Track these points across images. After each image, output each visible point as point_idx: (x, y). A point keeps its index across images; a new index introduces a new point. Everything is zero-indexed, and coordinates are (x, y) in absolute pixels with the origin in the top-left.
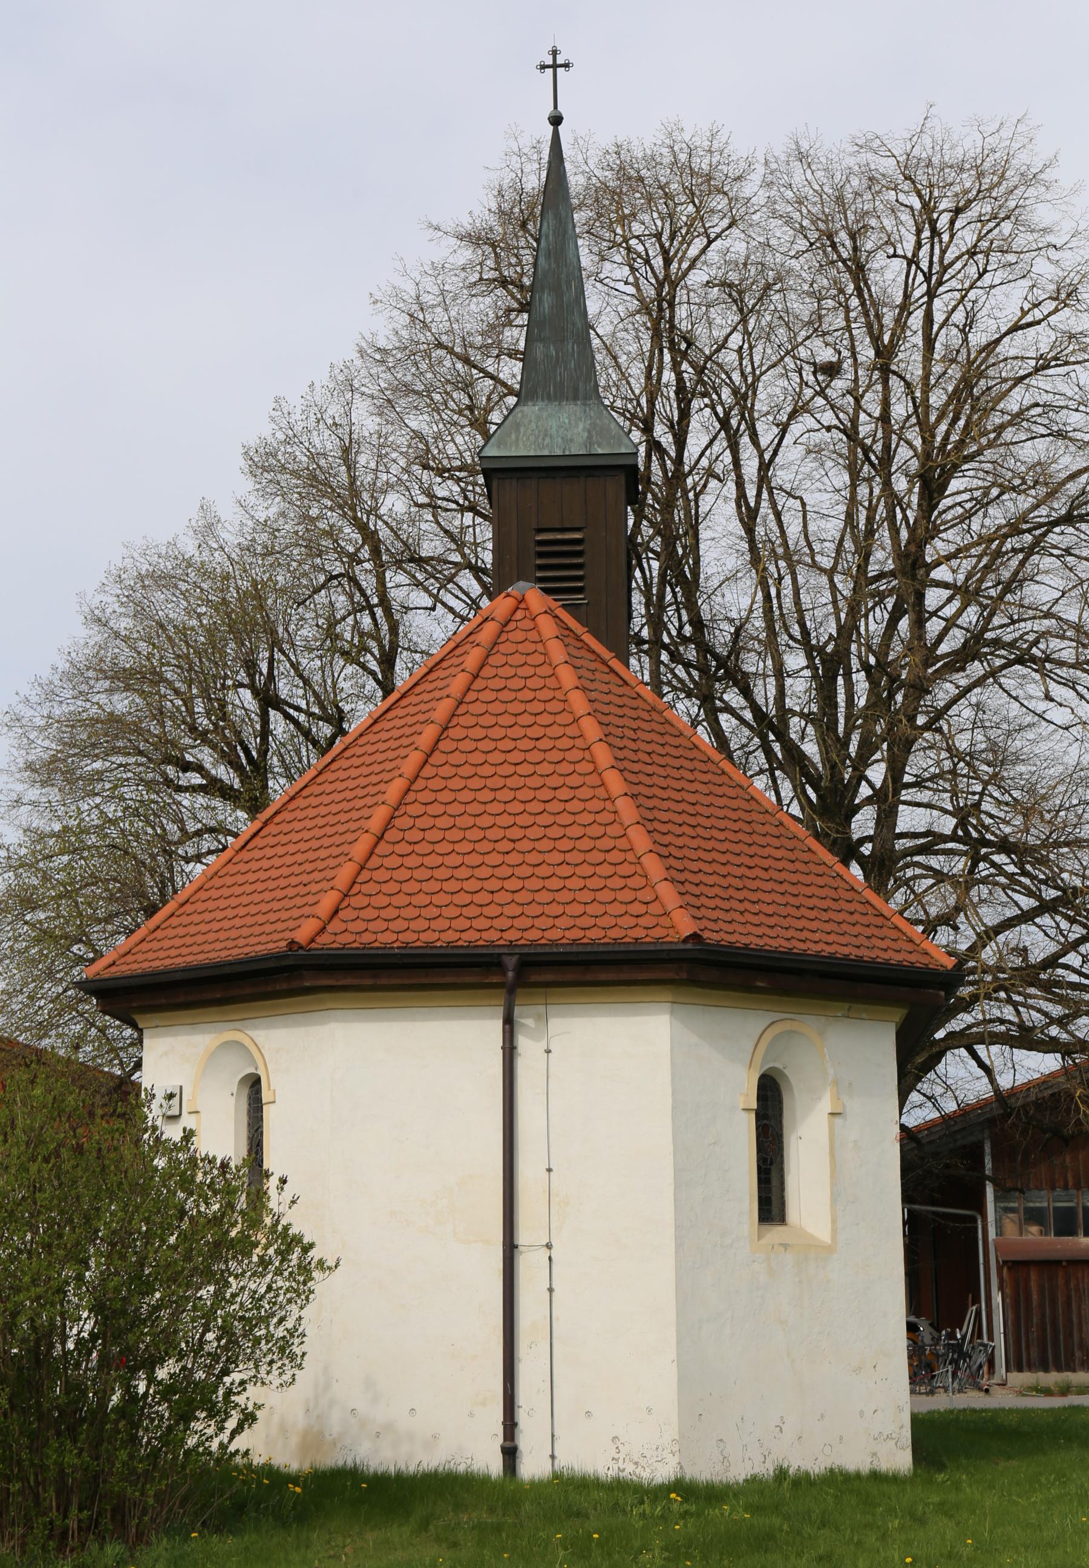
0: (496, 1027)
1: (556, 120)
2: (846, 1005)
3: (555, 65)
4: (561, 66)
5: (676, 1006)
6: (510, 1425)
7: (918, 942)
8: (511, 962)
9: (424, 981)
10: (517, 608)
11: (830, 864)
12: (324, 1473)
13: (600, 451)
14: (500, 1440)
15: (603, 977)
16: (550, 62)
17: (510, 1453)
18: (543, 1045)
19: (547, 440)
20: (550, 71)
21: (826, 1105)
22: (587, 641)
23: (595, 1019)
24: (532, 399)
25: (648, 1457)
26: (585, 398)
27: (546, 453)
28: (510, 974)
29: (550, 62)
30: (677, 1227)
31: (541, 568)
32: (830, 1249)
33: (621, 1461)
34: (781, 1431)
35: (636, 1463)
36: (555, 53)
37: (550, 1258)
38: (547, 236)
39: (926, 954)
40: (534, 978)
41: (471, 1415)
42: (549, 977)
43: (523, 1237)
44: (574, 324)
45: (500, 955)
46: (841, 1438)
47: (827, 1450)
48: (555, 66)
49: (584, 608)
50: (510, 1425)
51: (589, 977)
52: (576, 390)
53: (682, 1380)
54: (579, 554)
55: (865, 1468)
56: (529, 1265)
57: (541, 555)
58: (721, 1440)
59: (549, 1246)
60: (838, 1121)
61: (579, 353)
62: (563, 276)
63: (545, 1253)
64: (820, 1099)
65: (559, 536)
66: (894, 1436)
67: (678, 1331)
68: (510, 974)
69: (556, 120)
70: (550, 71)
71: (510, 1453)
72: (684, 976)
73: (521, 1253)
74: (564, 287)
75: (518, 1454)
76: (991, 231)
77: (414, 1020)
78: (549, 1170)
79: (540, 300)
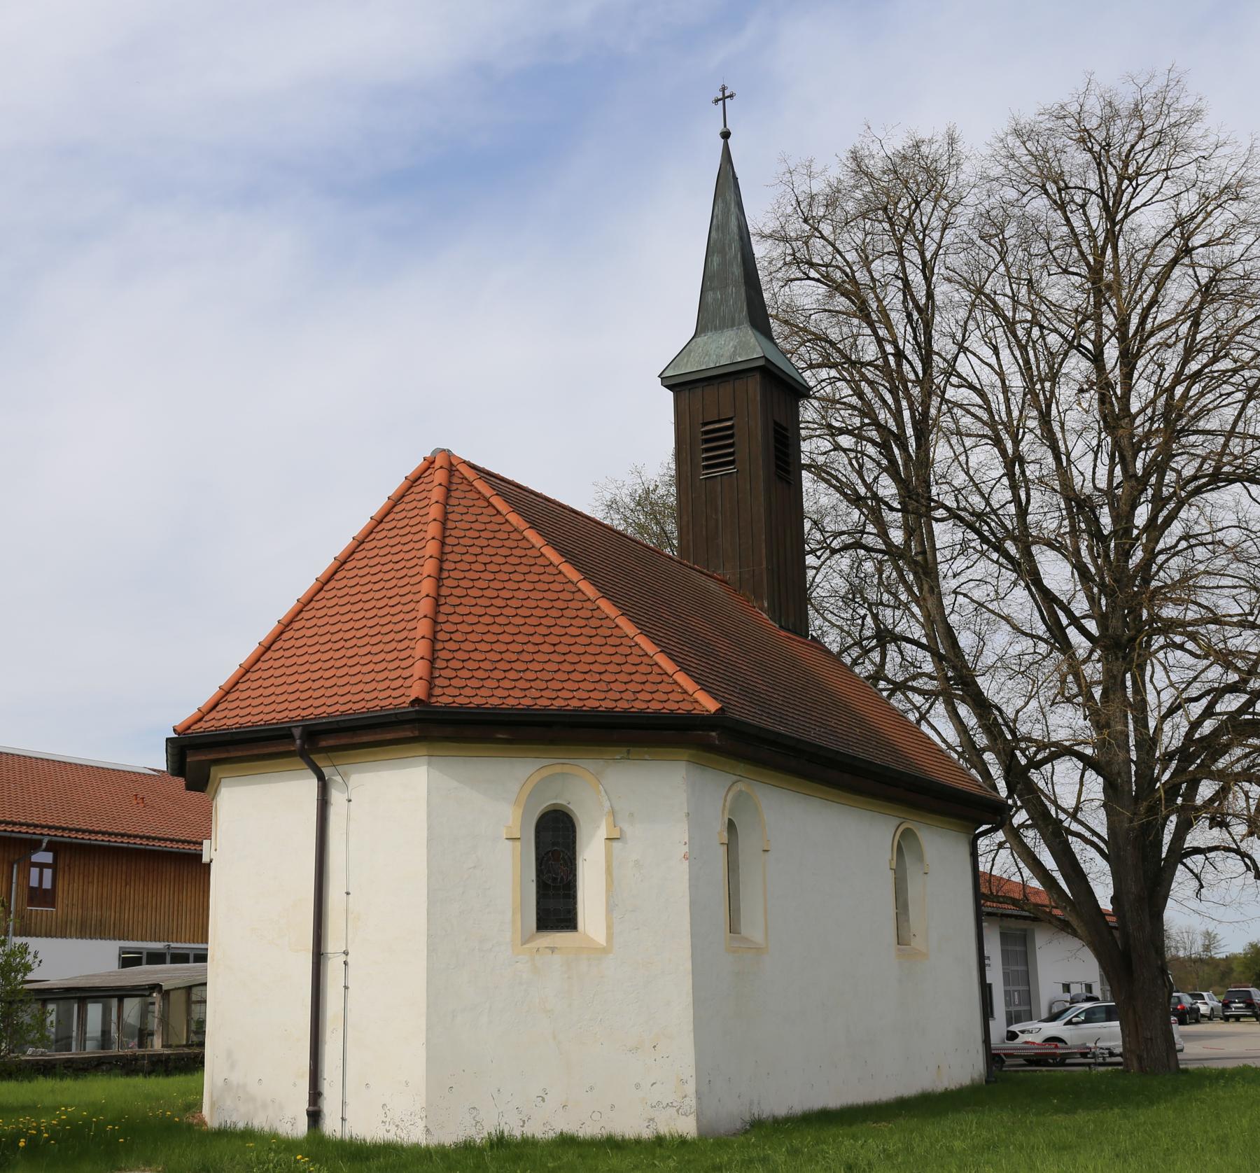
0: (312, 784)
1: (726, 135)
2: (625, 749)
3: (724, 97)
4: (728, 97)
5: (433, 758)
6: (315, 1094)
7: (691, 693)
8: (297, 732)
9: (256, 752)
10: (429, 468)
11: (631, 635)
12: (829, 1111)
13: (740, 360)
14: (306, 1106)
15: (365, 739)
16: (720, 96)
17: (315, 1116)
18: (346, 797)
19: (707, 358)
20: (721, 103)
21: (602, 833)
22: (480, 488)
23: (380, 773)
24: (704, 332)
25: (405, 1120)
26: (739, 325)
27: (704, 367)
28: (298, 742)
29: (721, 96)
30: (429, 936)
31: (707, 450)
32: (605, 951)
33: (387, 1123)
34: (543, 1100)
35: (397, 1126)
36: (723, 89)
37: (346, 963)
38: (717, 216)
39: (697, 702)
40: (323, 744)
41: (295, 1085)
42: (331, 742)
43: (333, 945)
44: (733, 273)
45: (290, 727)
46: (613, 1107)
47: (596, 1116)
48: (724, 99)
49: (735, 475)
50: (315, 1094)
51: (356, 740)
52: (733, 320)
53: (429, 1060)
54: (731, 436)
55: (647, 1134)
56: (333, 968)
57: (706, 441)
58: (474, 1108)
59: (346, 953)
60: (615, 844)
61: (736, 293)
62: (727, 242)
63: (343, 958)
64: (599, 827)
65: (717, 426)
66: (675, 1104)
67: (428, 1019)
68: (298, 742)
69: (726, 135)
70: (721, 103)
71: (315, 1116)
72: (417, 733)
73: (329, 959)
74: (727, 249)
75: (322, 1114)
76: (1149, 155)
77: (270, 783)
78: (348, 894)
79: (712, 261)
